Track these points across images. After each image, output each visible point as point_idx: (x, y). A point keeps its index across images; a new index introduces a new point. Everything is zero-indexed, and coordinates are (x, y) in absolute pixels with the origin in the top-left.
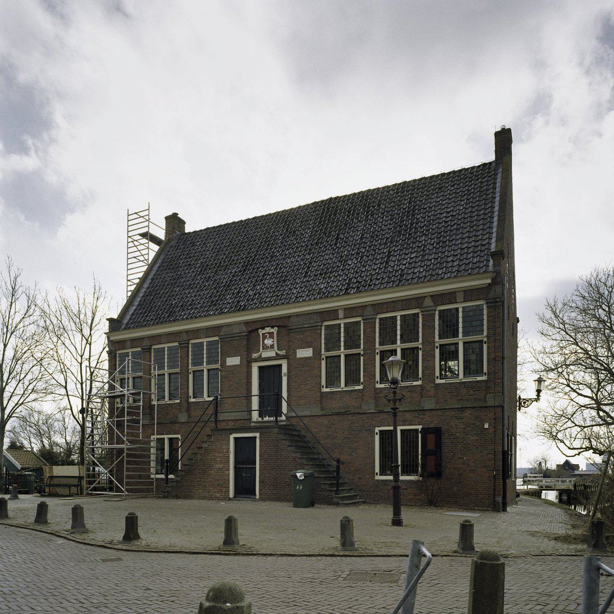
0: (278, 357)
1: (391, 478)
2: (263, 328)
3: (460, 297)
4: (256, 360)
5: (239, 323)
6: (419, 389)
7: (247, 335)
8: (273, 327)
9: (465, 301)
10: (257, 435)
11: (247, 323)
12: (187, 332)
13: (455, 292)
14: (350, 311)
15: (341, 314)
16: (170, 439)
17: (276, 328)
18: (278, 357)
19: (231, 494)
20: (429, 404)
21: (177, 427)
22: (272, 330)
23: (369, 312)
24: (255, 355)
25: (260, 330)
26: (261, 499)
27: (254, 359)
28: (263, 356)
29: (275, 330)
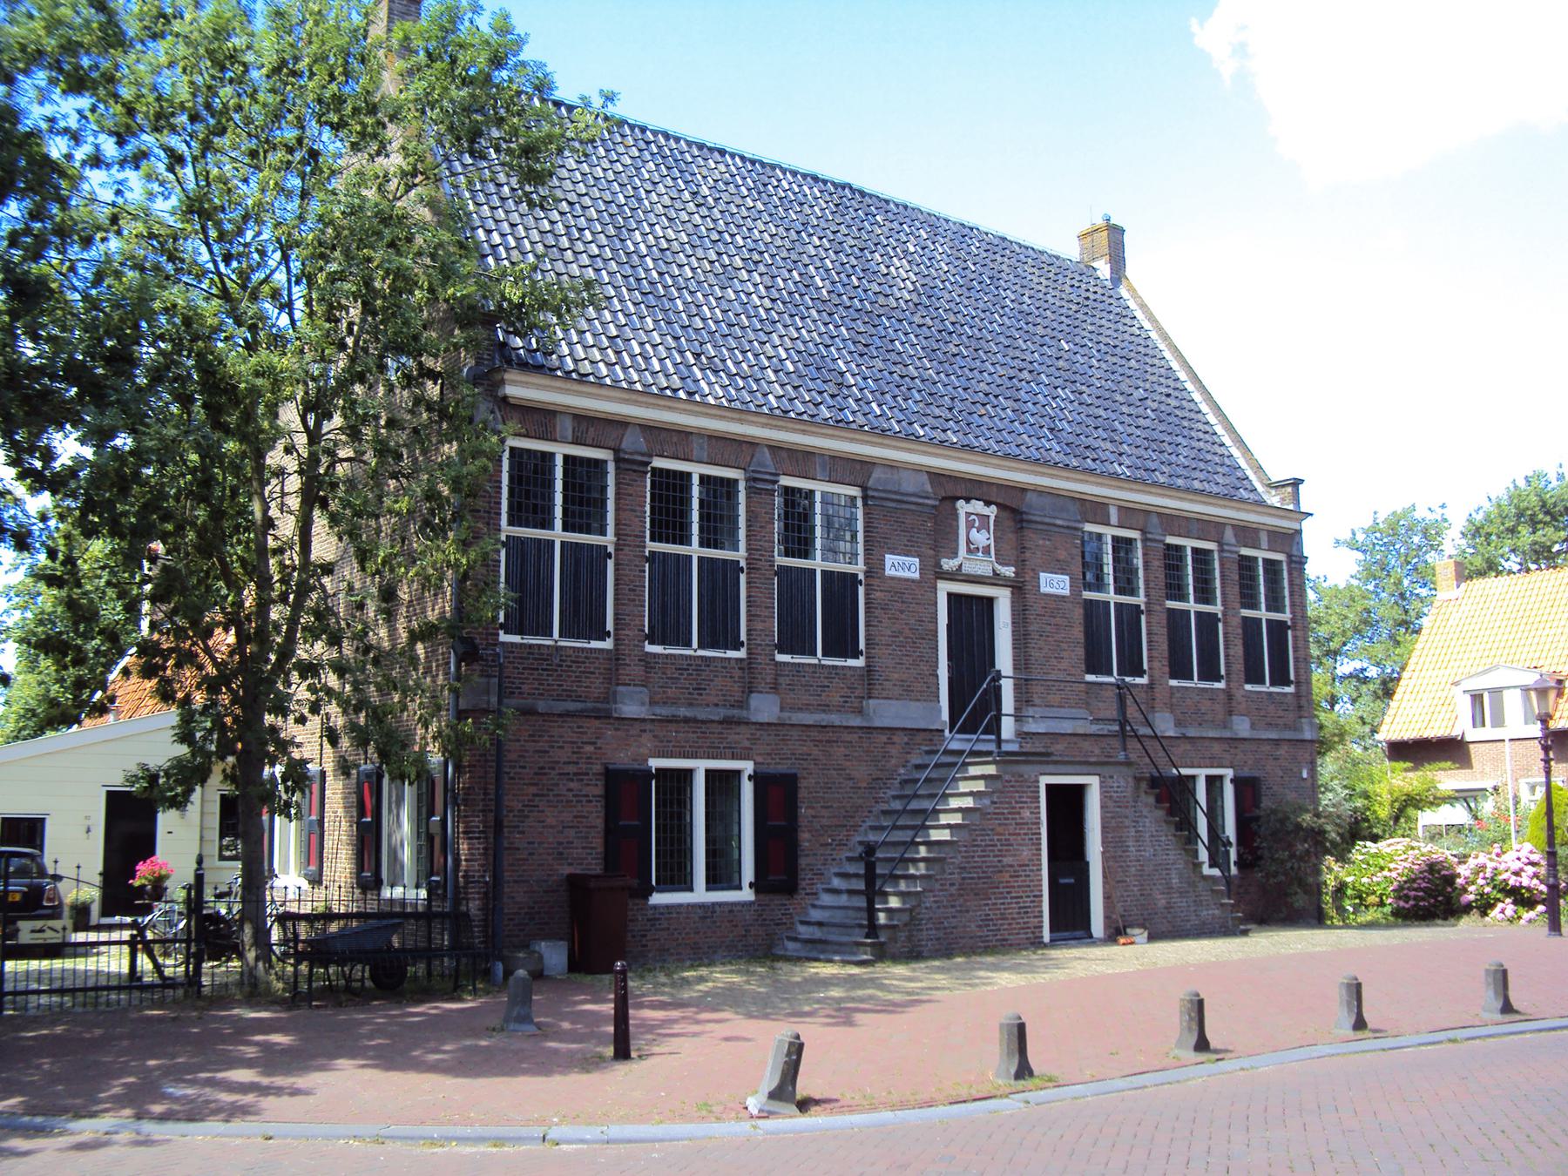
0: (996, 580)
1: (1062, 881)
2: (968, 500)
3: (566, 426)
4: (952, 576)
5: (917, 469)
6: (1222, 696)
7: (934, 507)
8: (988, 503)
9: (576, 442)
11: (936, 477)
12: (775, 449)
13: (554, 413)
14: (1130, 514)
15: (566, 426)
16: (1209, 779)
17: (994, 508)
18: (996, 580)
19: (1047, 936)
21: (741, 736)
23: (632, 442)
24: (948, 564)
25: (960, 503)
26: (1054, 943)
27: (947, 573)
28: (968, 568)
29: (992, 511)
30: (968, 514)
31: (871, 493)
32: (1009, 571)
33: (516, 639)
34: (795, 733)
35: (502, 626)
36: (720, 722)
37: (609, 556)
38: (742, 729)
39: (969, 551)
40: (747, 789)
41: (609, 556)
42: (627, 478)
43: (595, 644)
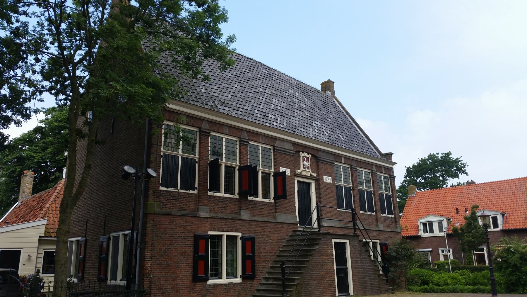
0: (311, 178)
6: (374, 217)
8: (308, 154)
10: (347, 241)
11: (294, 144)
18: (311, 178)
20: (381, 227)
22: (308, 156)
24: (298, 171)
25: (301, 153)
28: (303, 173)
29: (309, 156)
30: (303, 157)
31: (202, 130)
32: (315, 175)
33: (165, 189)
34: (254, 223)
35: (160, 184)
36: (231, 219)
37: (197, 162)
38: (238, 222)
39: (304, 168)
40: (239, 242)
41: (197, 162)
42: (242, 147)
43: (191, 192)
